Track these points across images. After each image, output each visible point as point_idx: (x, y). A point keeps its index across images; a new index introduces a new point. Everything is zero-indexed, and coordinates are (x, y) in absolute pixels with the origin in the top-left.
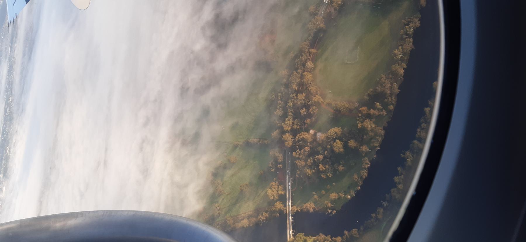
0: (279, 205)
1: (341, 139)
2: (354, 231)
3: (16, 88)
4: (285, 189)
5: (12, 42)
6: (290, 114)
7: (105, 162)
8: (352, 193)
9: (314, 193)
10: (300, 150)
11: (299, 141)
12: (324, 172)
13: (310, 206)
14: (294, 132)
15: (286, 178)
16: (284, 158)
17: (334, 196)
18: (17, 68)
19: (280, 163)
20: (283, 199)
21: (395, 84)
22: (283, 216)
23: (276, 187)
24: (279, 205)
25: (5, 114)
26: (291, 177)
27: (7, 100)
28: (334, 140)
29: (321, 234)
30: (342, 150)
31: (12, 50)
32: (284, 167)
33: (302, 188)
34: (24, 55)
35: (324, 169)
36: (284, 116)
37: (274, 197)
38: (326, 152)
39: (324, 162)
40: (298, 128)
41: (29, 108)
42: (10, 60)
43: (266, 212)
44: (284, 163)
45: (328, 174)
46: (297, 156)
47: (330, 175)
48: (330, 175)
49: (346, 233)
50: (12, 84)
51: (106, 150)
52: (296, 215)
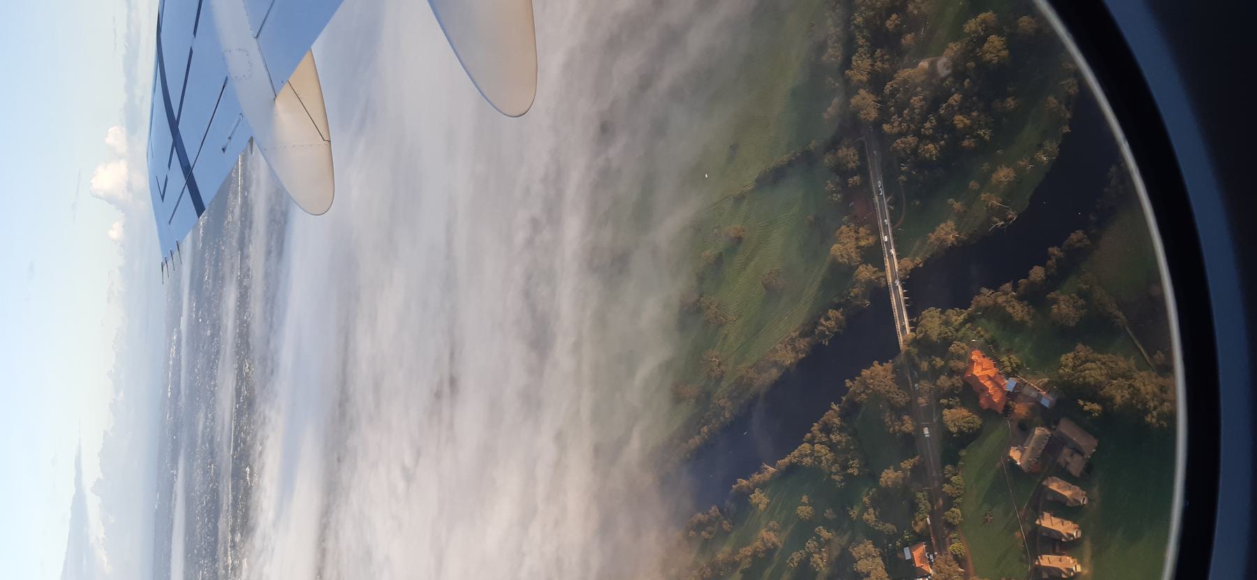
0: (865, 272)
1: (999, 32)
2: (1076, 236)
3: (257, 329)
4: (876, 232)
5: (242, 245)
6: (861, 41)
7: (453, 382)
8: (1052, 146)
10: (900, 115)
12: (969, 131)
13: (947, 232)
14: (877, 82)
16: (863, 158)
17: (1004, 174)
18: (257, 291)
20: (874, 255)
22: (880, 294)
23: (852, 233)
24: (865, 272)
25: (238, 402)
26: (887, 195)
27: (240, 369)
28: (983, 40)
29: (984, 290)
30: (1005, 53)
31: (244, 257)
32: (866, 183)
33: (922, 187)
34: (269, 253)
35: (968, 122)
36: (850, 47)
37: (850, 258)
39: (964, 109)
40: (886, 66)
41: (286, 357)
42: (240, 282)
43: (837, 307)
44: (862, 170)
45: (981, 132)
46: (896, 130)
47: (985, 133)
48: (985, 133)
49: (1054, 250)
50: (248, 335)
51: (452, 355)
52: (911, 282)
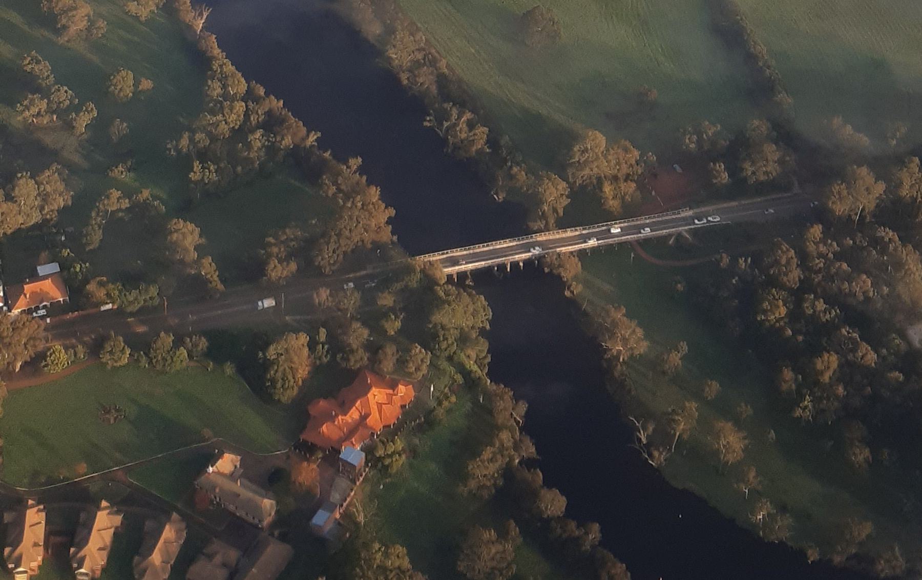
0: (555, 193)
4: (628, 212)
8: (782, 530)
9: (684, 347)
11: (876, 242)
12: (810, 381)
13: (627, 340)
15: (677, 208)
16: (761, 188)
17: (732, 443)
19: (734, 171)
20: (585, 208)
21: (848, 537)
22: (515, 220)
23: (625, 169)
24: (555, 193)
26: (695, 232)
33: (709, 297)
35: (826, 378)
38: (898, 376)
39: (850, 371)
43: (492, 142)
44: (739, 188)
46: (811, 248)
47: (806, 409)
48: (806, 409)
49: (594, 533)
